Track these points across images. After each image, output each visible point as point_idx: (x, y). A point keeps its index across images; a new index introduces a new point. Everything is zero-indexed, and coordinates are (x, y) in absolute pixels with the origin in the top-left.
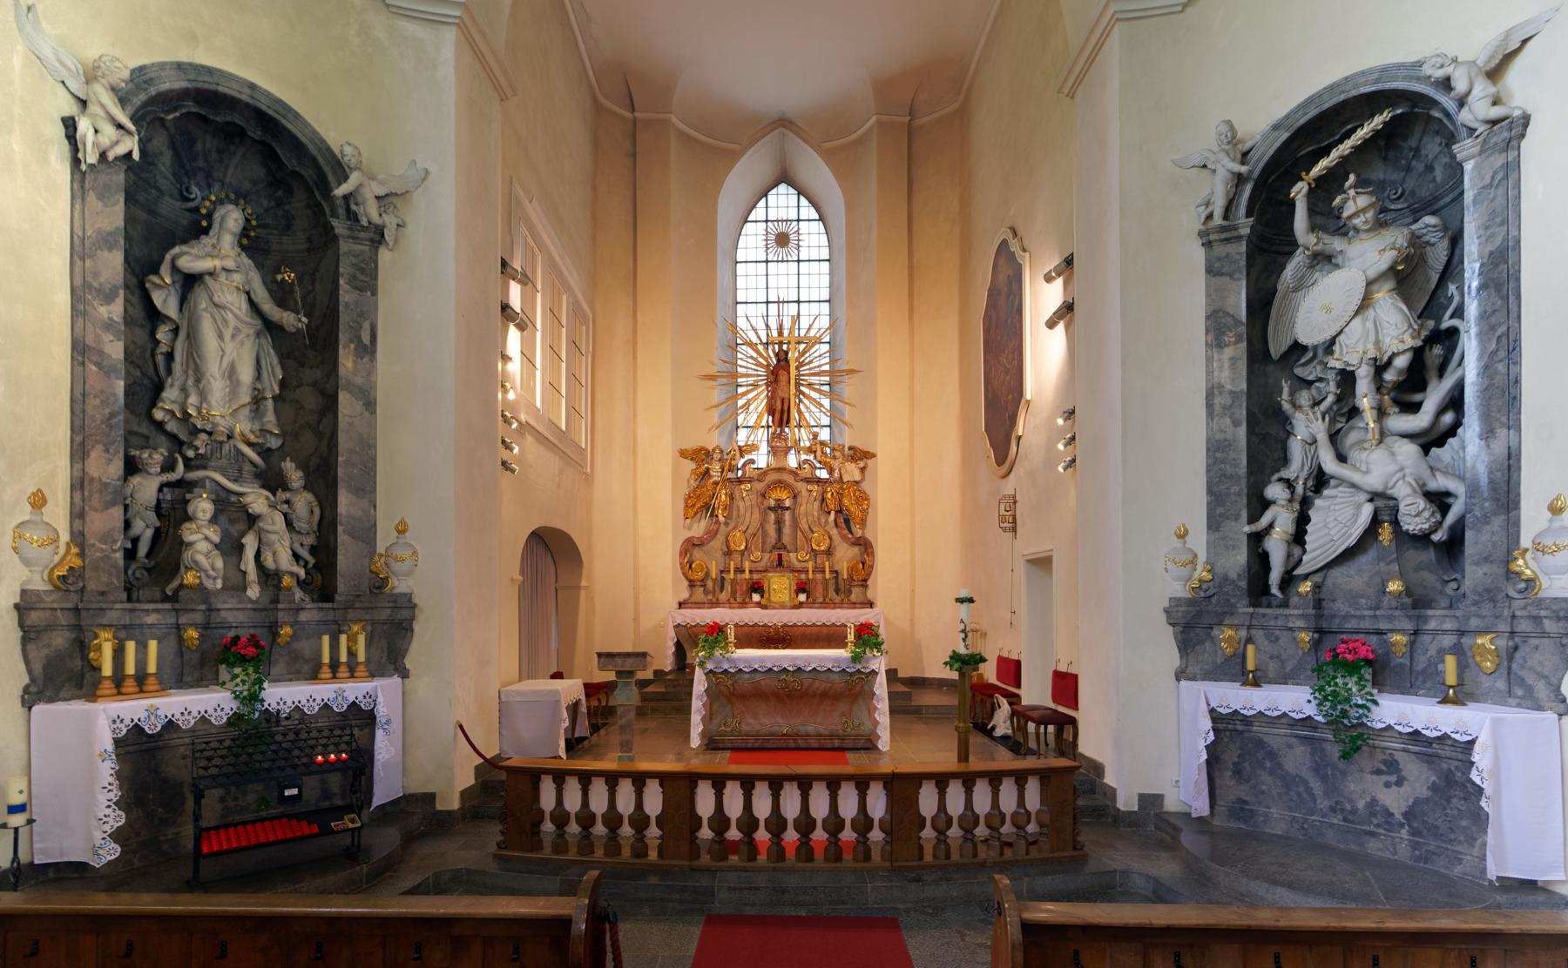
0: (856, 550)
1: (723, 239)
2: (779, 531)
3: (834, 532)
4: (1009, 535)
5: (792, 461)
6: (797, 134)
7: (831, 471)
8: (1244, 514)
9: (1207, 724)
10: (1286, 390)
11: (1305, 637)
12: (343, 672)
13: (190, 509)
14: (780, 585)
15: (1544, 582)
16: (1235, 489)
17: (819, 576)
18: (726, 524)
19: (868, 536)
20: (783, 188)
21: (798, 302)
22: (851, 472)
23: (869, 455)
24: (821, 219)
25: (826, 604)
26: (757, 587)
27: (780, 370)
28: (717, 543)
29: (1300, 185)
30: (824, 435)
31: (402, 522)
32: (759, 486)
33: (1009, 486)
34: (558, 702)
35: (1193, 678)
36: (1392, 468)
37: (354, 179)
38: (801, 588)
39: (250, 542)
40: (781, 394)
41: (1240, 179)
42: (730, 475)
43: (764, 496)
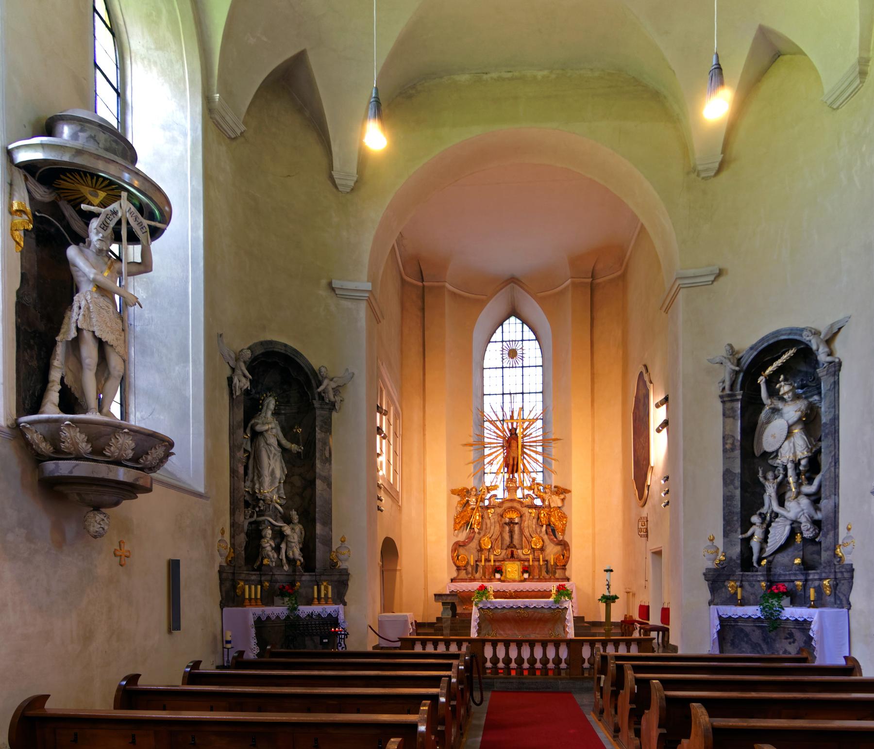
0: (559, 548)
1: (476, 355)
2: (511, 537)
3: (546, 537)
4: (644, 539)
5: (519, 494)
6: (522, 287)
7: (543, 501)
8: (739, 530)
9: (717, 622)
10: (761, 472)
11: (763, 584)
12: (323, 601)
13: (263, 534)
14: (512, 569)
15: (339, 564)
16: (735, 518)
17: (536, 563)
18: (479, 533)
19: (567, 539)
20: (513, 319)
21: (523, 393)
22: (556, 501)
23: (566, 491)
24: (537, 339)
25: (540, 580)
26: (498, 570)
27: (511, 440)
28: (474, 545)
29: (761, 378)
30: (539, 478)
31: (343, 537)
32: (499, 510)
33: (645, 512)
34: (407, 621)
35: (717, 604)
36: (799, 510)
37: (326, 382)
38: (525, 570)
39: (283, 546)
40: (512, 454)
41: (737, 373)
42: (481, 504)
43: (502, 516)
